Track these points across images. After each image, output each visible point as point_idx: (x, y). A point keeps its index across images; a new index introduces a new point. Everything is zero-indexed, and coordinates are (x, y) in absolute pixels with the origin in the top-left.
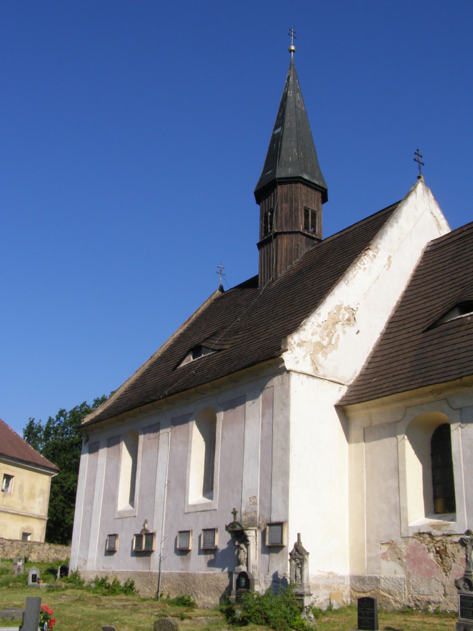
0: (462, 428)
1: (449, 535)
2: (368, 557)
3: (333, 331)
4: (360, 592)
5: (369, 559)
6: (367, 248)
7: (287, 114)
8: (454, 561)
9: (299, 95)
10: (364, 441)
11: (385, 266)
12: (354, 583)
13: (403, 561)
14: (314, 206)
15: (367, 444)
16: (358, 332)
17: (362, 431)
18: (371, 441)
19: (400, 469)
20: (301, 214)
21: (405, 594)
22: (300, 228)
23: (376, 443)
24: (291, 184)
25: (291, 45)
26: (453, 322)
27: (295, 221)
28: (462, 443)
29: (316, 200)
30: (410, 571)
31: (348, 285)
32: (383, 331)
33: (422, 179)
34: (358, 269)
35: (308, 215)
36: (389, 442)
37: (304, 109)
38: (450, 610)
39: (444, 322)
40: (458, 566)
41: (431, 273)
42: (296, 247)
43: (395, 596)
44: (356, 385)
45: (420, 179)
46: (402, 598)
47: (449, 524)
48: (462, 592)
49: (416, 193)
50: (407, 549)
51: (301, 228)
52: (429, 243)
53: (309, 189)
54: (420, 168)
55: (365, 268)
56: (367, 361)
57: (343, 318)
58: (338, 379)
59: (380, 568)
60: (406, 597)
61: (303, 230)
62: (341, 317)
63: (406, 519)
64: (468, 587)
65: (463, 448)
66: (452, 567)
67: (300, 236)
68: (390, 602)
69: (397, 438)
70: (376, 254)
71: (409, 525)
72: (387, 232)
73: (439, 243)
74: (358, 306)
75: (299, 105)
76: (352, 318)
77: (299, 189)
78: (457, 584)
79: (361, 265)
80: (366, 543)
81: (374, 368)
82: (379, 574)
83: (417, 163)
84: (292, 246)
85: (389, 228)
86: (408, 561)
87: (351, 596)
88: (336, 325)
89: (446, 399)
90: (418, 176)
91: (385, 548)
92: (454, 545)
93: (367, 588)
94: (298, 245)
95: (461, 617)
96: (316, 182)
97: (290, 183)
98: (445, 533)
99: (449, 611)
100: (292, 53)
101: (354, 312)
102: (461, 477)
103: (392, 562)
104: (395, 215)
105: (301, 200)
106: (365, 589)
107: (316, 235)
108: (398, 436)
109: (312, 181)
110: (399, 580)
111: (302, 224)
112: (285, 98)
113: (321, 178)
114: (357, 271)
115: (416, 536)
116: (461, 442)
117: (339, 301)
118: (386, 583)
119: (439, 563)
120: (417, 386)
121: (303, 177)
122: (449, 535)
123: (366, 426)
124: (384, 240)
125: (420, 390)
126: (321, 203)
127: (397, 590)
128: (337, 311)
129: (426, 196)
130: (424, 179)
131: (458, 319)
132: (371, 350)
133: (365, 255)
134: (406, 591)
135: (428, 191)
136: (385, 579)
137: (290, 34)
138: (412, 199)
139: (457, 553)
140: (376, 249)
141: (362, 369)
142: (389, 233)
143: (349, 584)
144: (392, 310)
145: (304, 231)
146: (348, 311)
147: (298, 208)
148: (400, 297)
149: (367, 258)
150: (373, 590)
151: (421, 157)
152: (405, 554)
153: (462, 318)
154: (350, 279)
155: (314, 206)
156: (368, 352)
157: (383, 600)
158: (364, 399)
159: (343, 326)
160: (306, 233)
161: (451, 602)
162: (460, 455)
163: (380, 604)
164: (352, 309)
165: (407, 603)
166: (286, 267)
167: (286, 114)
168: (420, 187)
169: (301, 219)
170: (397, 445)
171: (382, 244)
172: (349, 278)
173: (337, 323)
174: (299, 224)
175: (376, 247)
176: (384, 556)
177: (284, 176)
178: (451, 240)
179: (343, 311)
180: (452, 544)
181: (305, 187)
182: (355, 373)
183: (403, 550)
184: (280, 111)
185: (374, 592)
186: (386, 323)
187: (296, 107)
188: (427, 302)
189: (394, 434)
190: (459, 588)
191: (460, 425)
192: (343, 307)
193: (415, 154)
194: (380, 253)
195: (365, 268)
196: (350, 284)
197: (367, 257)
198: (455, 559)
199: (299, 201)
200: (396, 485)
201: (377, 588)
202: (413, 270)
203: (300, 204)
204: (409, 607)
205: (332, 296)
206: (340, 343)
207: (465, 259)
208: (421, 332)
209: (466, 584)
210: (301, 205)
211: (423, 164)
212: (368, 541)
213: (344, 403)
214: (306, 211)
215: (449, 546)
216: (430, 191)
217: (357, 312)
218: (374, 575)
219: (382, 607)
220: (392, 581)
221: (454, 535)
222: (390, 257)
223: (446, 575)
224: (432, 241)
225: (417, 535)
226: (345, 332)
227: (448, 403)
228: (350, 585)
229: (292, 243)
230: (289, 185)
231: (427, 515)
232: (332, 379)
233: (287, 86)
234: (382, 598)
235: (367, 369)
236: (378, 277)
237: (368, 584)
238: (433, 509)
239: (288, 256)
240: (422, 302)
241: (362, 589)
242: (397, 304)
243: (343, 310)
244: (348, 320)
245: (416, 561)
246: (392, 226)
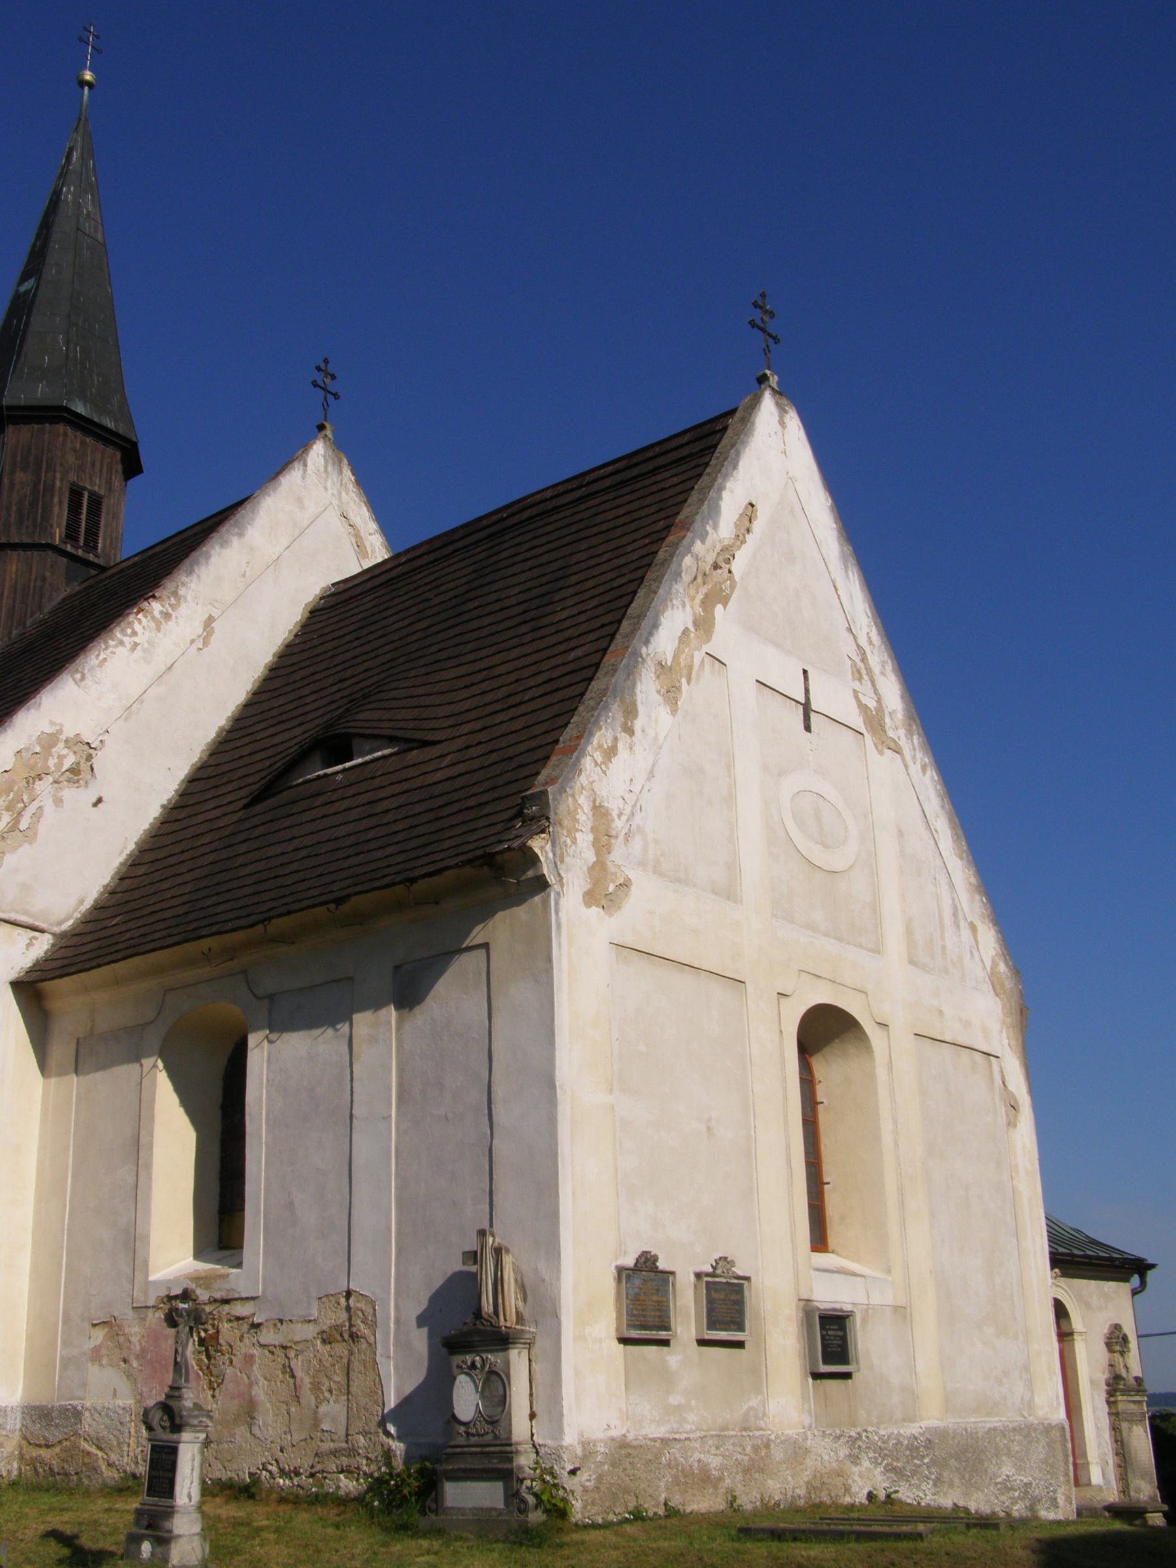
0: (271, 1042)
1: (226, 1301)
2: (62, 1357)
3: (25, 798)
4: (39, 1446)
5: (66, 1363)
6: (151, 594)
7: (55, 246)
8: (231, 1362)
9: (93, 200)
10: (76, 1072)
11: (193, 641)
12: (30, 1425)
13: (131, 1366)
14: (97, 481)
15: (81, 1077)
16: (100, 800)
17: (74, 1046)
18: (88, 1073)
19: (142, 1141)
20: (60, 502)
21: (129, 1446)
22: (53, 536)
23: (99, 1075)
24: (42, 423)
25: (84, 67)
26: (307, 786)
27: (42, 516)
28: (268, 1081)
29: (105, 469)
30: (145, 1389)
31: (83, 684)
32: (169, 800)
33: (328, 432)
34: (116, 646)
35: (80, 505)
36: (125, 1072)
37: (100, 237)
38: (214, 1477)
39: (289, 784)
40: (236, 1375)
41: (307, 663)
42: (39, 583)
43: (109, 1452)
44: (77, 931)
45: (324, 432)
46: (122, 1456)
47: (228, 1275)
48: (157, 1438)
49: (305, 465)
50: (143, 1336)
51: (57, 535)
52: (325, 589)
53: (88, 440)
54: (325, 405)
55: (136, 645)
56: (116, 873)
57: (59, 765)
58: (31, 916)
59: (84, 1385)
60: (131, 1454)
61: (61, 540)
62: (52, 762)
63: (146, 1263)
64: (167, 1424)
65: (268, 1092)
66: (226, 1376)
67: (51, 556)
68: (98, 1466)
69: (141, 1065)
70: (170, 611)
71: (151, 1278)
72: (208, 557)
73: (345, 591)
74: (106, 737)
75: (87, 225)
76: (85, 767)
77: (61, 438)
78: (147, 1418)
79: (126, 635)
80: (60, 1324)
81: (127, 891)
82: (82, 1399)
83: (322, 392)
84: (30, 580)
85: (217, 548)
86: (141, 1365)
87: (21, 1457)
88: (38, 783)
89: (244, 972)
90: (320, 423)
91: (99, 1335)
92: (235, 1324)
93: (54, 1435)
94: (44, 579)
95: (148, 1495)
96: (109, 424)
97: (40, 420)
98: (218, 1295)
99: (210, 1479)
100: (86, 89)
101: (92, 751)
102: (260, 1162)
103: (110, 1368)
104: (238, 516)
105: (62, 465)
106: (51, 1439)
107: (96, 556)
108: (144, 1061)
109: (96, 420)
110: (121, 1412)
111: (59, 526)
112: (55, 201)
113: (124, 412)
114: (110, 650)
115: (162, 1305)
116: (265, 1077)
117: (52, 723)
118: (94, 1420)
119: (201, 1369)
120: (181, 937)
121: (73, 409)
122: (226, 1301)
123: (82, 1036)
124: (199, 577)
125: (190, 947)
126: (120, 476)
127: (115, 1436)
128: (43, 747)
129: (334, 475)
130: (333, 432)
131: (319, 777)
132: (131, 846)
133: (138, 613)
134: (132, 1439)
135: (340, 461)
136: (94, 1410)
137: (86, 40)
138: (292, 479)
139: (239, 1343)
140: (172, 599)
141: (102, 894)
142: (214, 560)
143: (18, 1426)
144: (203, 751)
145: (65, 543)
146: (76, 748)
147: (53, 486)
148: (228, 719)
149: (144, 620)
150: (66, 1439)
151: (333, 377)
152: (138, 1348)
153: (326, 775)
154: (89, 670)
155: (97, 481)
156: (122, 852)
157: (84, 1464)
158: (73, 969)
159: (57, 785)
160: (69, 548)
161: (216, 1458)
162: (261, 1107)
163: (77, 1473)
164: (88, 744)
165: (130, 1468)
166: (10, 633)
167: (51, 244)
168: (318, 451)
169: (60, 514)
170: (141, 1083)
171: (193, 586)
172: (87, 667)
173: (40, 778)
174: (52, 526)
175: (175, 593)
176: (96, 1355)
177: (22, 403)
178: (370, 585)
179: (60, 749)
180: (231, 1321)
181: (79, 433)
182: (82, 902)
183: (134, 1339)
184: (38, 237)
185: (68, 1443)
186: (183, 781)
187: (78, 229)
188: (276, 734)
189: (137, 1059)
190: (150, 1428)
191: (267, 1037)
192: (63, 737)
193: (319, 369)
194: (183, 610)
195: (136, 645)
196: (89, 681)
197: (146, 617)
198: (233, 1357)
199: (58, 468)
200: (131, 1180)
201: (76, 1434)
202: (274, 655)
203: (58, 475)
204: (134, 1476)
205: (33, 711)
206: (42, 828)
207: (380, 633)
208: (241, 806)
209: (165, 1418)
210: (62, 479)
211: (336, 396)
212: (66, 1320)
213: (34, 976)
214: (76, 494)
215: (225, 1327)
216: (345, 461)
217: (99, 753)
218: (72, 1402)
219: (80, 1480)
220: (107, 1415)
221: (236, 1299)
222: (210, 620)
223: (213, 1396)
224: (333, 585)
225: (164, 1303)
226: (62, 801)
227: (247, 982)
228: (21, 1430)
229: (31, 573)
230: (36, 426)
231: (199, 1254)
232: (12, 916)
233: (63, 175)
234: (83, 1456)
235: (113, 893)
236: (170, 668)
237: (57, 1426)
238: (215, 1239)
239: (16, 605)
240: (268, 732)
241: (45, 1438)
242: (218, 735)
243: (61, 745)
244: (74, 771)
245: (157, 1366)
246: (225, 544)
